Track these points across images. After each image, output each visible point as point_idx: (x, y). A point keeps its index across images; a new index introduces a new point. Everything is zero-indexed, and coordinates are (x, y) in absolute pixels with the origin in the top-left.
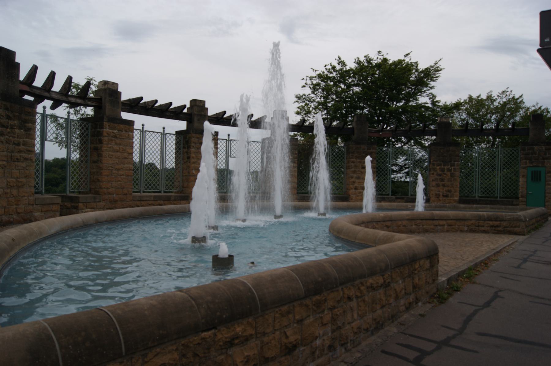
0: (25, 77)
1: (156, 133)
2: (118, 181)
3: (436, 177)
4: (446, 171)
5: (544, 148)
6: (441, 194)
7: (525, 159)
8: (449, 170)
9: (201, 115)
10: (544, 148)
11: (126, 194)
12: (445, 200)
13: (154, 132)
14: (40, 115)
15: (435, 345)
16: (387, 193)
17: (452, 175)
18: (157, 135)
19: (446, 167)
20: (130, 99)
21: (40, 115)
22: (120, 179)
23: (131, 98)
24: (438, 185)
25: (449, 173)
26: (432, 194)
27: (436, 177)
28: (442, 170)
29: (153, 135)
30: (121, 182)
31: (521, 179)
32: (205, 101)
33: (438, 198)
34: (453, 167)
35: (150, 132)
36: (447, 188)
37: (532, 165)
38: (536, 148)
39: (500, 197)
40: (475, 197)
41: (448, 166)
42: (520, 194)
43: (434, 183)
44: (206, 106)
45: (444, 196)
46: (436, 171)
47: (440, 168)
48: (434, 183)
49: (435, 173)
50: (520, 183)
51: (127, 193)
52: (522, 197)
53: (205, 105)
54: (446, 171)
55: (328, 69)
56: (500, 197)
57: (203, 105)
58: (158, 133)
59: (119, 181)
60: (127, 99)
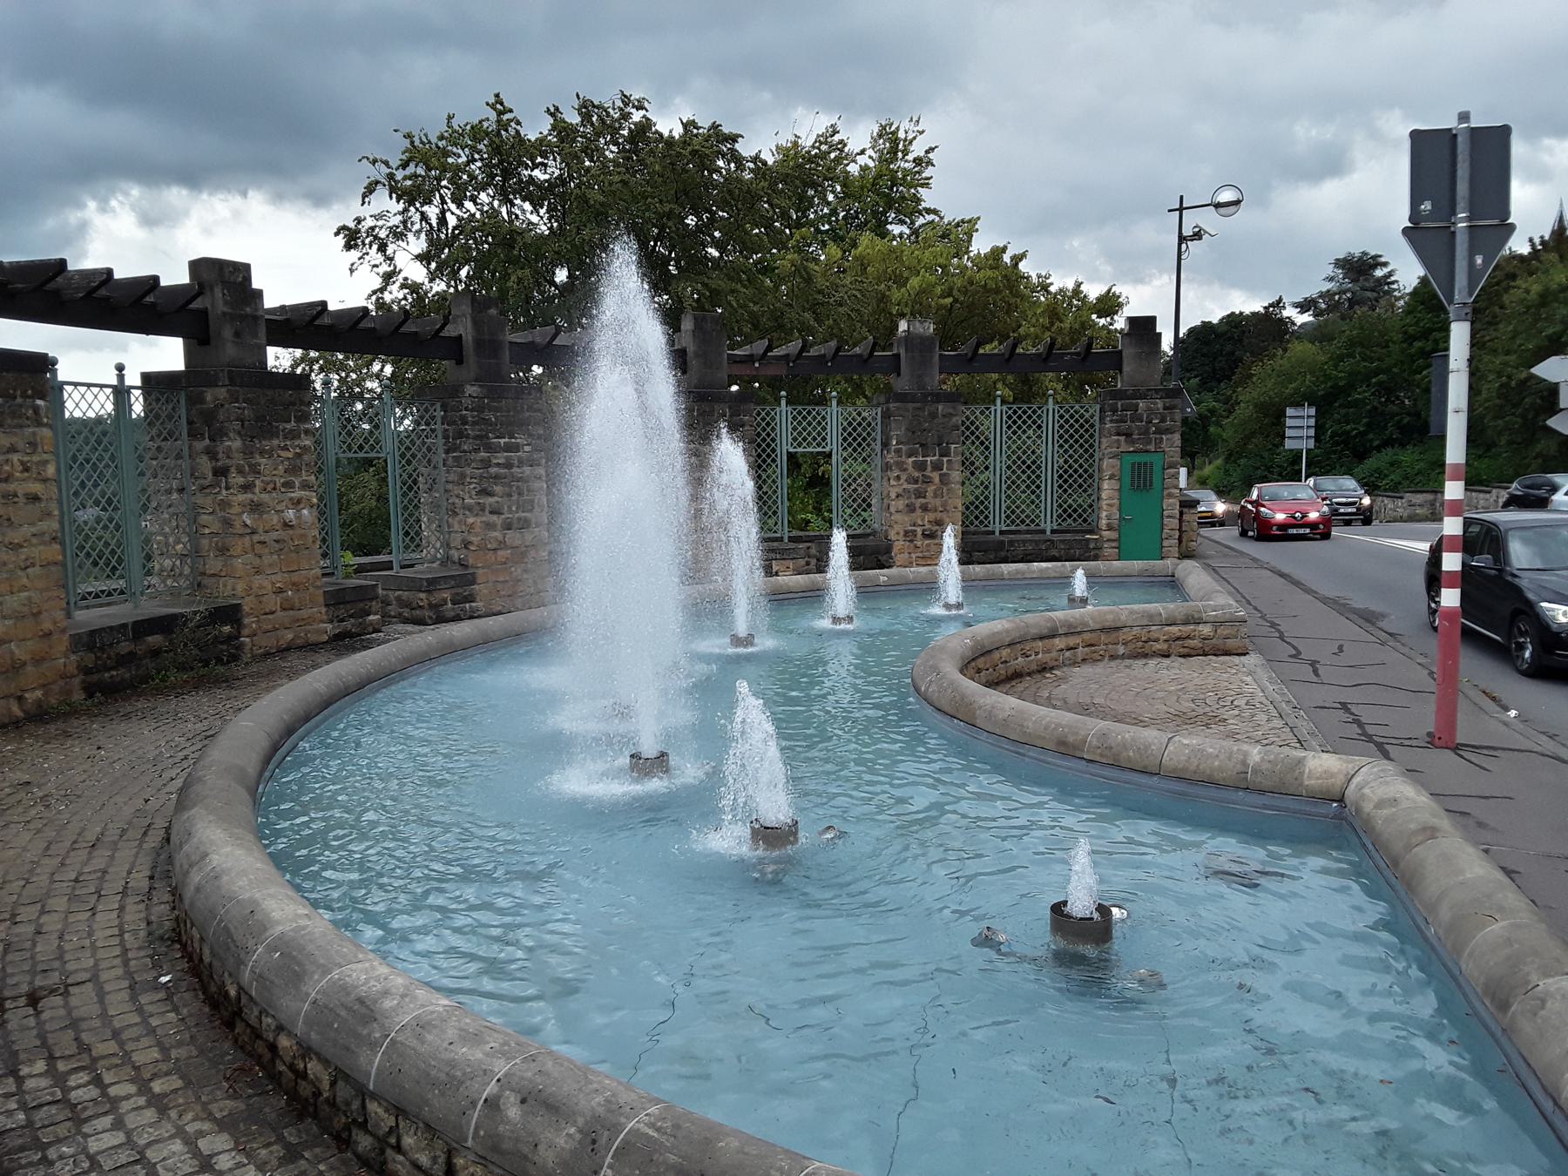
0: (351, 309)
1: (96, 390)
2: (19, 591)
3: (906, 486)
4: (929, 468)
5: (1160, 404)
6: (919, 530)
7: (1118, 434)
8: (937, 467)
9: (243, 318)
10: (1160, 404)
11: (48, 635)
12: (928, 545)
13: (89, 385)
14: (111, 390)
15: (1513, 875)
16: (776, 535)
17: (944, 480)
18: (102, 397)
19: (929, 459)
20: (283, 307)
21: (111, 390)
22: (25, 581)
23: (288, 303)
24: (911, 508)
25: (936, 476)
26: (898, 533)
27: (906, 486)
28: (921, 466)
29: (89, 396)
30: (29, 590)
31: (1105, 485)
32: (247, 267)
33: (911, 541)
34: (945, 459)
35: (76, 384)
36: (930, 516)
37: (1132, 449)
38: (1142, 404)
39: (1053, 531)
40: (993, 533)
41: (935, 455)
42: (1104, 522)
43: (901, 504)
44: (255, 285)
45: (925, 536)
46: (905, 470)
47: (913, 462)
48: (901, 504)
49: (904, 477)
50: (1104, 495)
51: (51, 628)
52: (1110, 528)
53: (248, 279)
54: (929, 468)
55: (1131, 310)
56: (1053, 531)
57: (244, 277)
58: (102, 386)
59: (24, 588)
60: (277, 304)
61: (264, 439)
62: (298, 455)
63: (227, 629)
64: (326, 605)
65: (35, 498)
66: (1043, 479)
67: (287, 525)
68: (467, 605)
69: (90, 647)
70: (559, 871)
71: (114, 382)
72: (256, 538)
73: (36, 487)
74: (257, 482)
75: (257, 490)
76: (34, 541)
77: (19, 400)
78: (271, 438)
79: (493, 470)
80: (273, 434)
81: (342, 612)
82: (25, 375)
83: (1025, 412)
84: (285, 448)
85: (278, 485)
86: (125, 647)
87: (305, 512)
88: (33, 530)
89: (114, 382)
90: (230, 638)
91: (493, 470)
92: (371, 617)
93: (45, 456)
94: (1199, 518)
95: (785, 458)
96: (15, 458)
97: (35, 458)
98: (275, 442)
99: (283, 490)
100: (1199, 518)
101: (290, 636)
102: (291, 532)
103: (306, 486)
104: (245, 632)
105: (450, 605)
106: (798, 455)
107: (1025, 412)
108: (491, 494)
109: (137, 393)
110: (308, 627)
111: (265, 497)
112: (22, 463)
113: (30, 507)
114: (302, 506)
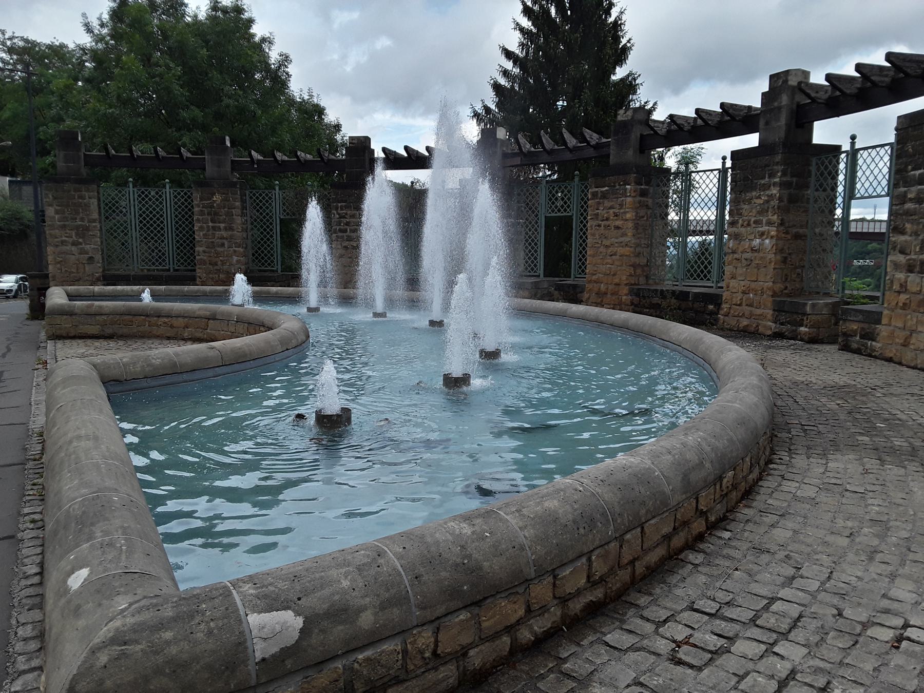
61: (748, 192)
62: (767, 202)
63: (711, 307)
64: (774, 310)
65: (617, 228)
66: (274, 231)
67: (753, 250)
68: (869, 343)
69: (637, 295)
70: (871, 632)
71: (720, 167)
72: (736, 256)
73: (618, 223)
74: (740, 221)
75: (739, 225)
76: (616, 245)
77: (618, 187)
78: (751, 191)
79: (909, 206)
80: (752, 188)
81: (783, 318)
82: (621, 176)
83: (261, 195)
84: (759, 197)
85: (752, 222)
86: (656, 300)
87: (767, 241)
88: (617, 241)
89: (720, 167)
90: (711, 313)
91: (909, 206)
92: (802, 329)
93: (627, 210)
94: (318, 465)
95: (278, 222)
96: (611, 211)
97: (622, 211)
98: (754, 194)
99: (754, 226)
100: (318, 465)
101: (745, 323)
102: (756, 254)
103: (769, 223)
104: (722, 312)
105: (858, 338)
106: (665, 189)
107: (261, 195)
108: (903, 232)
109: (730, 170)
110: (760, 322)
111: (743, 230)
112: (614, 213)
113: (616, 231)
114: (765, 237)
